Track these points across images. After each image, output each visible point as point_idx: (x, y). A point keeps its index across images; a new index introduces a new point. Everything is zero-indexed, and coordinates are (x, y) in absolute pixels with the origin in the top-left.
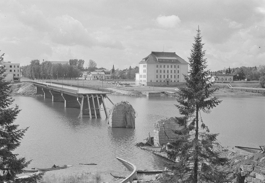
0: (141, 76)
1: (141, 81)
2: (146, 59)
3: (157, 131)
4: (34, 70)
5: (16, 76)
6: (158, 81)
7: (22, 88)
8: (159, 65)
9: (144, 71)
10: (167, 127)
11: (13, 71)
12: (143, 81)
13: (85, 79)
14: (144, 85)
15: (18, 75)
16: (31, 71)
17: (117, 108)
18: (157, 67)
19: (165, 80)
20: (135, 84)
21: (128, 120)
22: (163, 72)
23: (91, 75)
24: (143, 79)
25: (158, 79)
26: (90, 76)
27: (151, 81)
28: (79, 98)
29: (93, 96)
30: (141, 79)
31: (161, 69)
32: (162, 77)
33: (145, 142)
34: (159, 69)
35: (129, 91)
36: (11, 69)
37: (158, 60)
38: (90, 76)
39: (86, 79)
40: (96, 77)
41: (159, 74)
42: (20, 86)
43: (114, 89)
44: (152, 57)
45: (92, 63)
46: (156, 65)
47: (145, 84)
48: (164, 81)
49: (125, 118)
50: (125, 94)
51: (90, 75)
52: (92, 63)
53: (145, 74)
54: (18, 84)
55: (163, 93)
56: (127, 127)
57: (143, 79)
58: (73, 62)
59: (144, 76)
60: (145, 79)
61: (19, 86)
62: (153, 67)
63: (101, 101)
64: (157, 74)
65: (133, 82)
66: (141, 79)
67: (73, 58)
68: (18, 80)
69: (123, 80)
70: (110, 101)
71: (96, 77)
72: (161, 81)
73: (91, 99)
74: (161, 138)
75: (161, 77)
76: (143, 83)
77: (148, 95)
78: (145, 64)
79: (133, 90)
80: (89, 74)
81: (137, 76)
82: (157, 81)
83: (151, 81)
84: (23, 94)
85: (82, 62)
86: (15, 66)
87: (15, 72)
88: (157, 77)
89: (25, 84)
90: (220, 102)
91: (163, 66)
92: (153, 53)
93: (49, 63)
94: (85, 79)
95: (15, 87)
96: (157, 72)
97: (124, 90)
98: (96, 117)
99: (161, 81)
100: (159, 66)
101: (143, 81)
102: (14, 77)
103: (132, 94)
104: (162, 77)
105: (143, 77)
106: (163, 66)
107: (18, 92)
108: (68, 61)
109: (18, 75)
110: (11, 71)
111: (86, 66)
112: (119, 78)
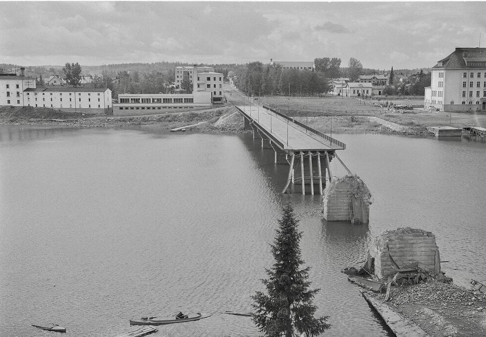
0: (434, 93)
1: (433, 102)
2: (444, 62)
3: (379, 251)
4: (251, 81)
5: (218, 95)
6: (466, 103)
7: (223, 118)
8: (468, 73)
9: (440, 84)
10: (398, 246)
11: (212, 86)
12: (437, 102)
13: (339, 95)
14: (438, 110)
15: (220, 92)
16: (247, 82)
17: (337, 188)
18: (465, 76)
19: (479, 100)
20: (423, 106)
21: (356, 210)
22: (475, 85)
23: (347, 88)
24: (437, 99)
25: (465, 99)
26: (346, 90)
27: (452, 103)
28: (289, 156)
29: (310, 154)
30: (434, 98)
31: (471, 80)
32: (474, 94)
33: (358, 268)
34: (468, 80)
35: (405, 125)
36: (209, 83)
37: (466, 63)
38: (346, 90)
39: (341, 94)
40: (356, 92)
41: (468, 89)
42: (221, 114)
43: (379, 119)
44: (455, 59)
45: (353, 62)
46: (462, 72)
47: (441, 107)
48: (478, 103)
49: (351, 207)
50: (397, 130)
51: (346, 87)
52: (353, 62)
53: (442, 89)
54: (217, 109)
55: (468, 129)
56: (353, 221)
57: (437, 99)
58: (321, 64)
59: (440, 94)
60: (441, 99)
61: (220, 113)
62: (457, 77)
63: (324, 166)
64: (463, 90)
65: (418, 102)
66: (434, 98)
67: (321, 57)
68: (220, 100)
69: (406, 96)
70: (342, 162)
71: (356, 92)
72: (471, 103)
73: (306, 159)
74: (384, 264)
75: (471, 95)
76: (437, 107)
77: (437, 135)
78: (442, 71)
79: (412, 124)
80: (345, 86)
81: (428, 91)
82: (464, 103)
83: (452, 103)
84: (223, 129)
85: (337, 61)
86: (219, 79)
87: (215, 89)
88: (464, 95)
89: (229, 109)
90: (326, 319)
91: (475, 75)
92: (459, 51)
93: (278, 67)
94: (339, 95)
95: (213, 116)
96: (464, 85)
97: (395, 123)
98: (313, 193)
99: (471, 103)
100: (468, 74)
101: (437, 102)
102: (214, 96)
103: (410, 131)
104: (474, 94)
105: (437, 96)
106: (475, 75)
107: (216, 125)
108: (313, 61)
109: (220, 92)
110: (209, 86)
111: (345, 65)
112: (397, 94)
